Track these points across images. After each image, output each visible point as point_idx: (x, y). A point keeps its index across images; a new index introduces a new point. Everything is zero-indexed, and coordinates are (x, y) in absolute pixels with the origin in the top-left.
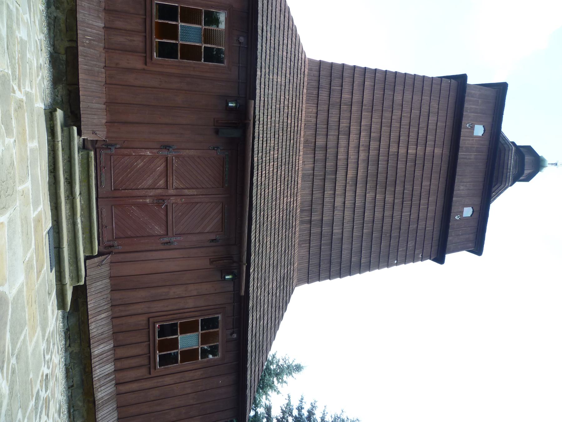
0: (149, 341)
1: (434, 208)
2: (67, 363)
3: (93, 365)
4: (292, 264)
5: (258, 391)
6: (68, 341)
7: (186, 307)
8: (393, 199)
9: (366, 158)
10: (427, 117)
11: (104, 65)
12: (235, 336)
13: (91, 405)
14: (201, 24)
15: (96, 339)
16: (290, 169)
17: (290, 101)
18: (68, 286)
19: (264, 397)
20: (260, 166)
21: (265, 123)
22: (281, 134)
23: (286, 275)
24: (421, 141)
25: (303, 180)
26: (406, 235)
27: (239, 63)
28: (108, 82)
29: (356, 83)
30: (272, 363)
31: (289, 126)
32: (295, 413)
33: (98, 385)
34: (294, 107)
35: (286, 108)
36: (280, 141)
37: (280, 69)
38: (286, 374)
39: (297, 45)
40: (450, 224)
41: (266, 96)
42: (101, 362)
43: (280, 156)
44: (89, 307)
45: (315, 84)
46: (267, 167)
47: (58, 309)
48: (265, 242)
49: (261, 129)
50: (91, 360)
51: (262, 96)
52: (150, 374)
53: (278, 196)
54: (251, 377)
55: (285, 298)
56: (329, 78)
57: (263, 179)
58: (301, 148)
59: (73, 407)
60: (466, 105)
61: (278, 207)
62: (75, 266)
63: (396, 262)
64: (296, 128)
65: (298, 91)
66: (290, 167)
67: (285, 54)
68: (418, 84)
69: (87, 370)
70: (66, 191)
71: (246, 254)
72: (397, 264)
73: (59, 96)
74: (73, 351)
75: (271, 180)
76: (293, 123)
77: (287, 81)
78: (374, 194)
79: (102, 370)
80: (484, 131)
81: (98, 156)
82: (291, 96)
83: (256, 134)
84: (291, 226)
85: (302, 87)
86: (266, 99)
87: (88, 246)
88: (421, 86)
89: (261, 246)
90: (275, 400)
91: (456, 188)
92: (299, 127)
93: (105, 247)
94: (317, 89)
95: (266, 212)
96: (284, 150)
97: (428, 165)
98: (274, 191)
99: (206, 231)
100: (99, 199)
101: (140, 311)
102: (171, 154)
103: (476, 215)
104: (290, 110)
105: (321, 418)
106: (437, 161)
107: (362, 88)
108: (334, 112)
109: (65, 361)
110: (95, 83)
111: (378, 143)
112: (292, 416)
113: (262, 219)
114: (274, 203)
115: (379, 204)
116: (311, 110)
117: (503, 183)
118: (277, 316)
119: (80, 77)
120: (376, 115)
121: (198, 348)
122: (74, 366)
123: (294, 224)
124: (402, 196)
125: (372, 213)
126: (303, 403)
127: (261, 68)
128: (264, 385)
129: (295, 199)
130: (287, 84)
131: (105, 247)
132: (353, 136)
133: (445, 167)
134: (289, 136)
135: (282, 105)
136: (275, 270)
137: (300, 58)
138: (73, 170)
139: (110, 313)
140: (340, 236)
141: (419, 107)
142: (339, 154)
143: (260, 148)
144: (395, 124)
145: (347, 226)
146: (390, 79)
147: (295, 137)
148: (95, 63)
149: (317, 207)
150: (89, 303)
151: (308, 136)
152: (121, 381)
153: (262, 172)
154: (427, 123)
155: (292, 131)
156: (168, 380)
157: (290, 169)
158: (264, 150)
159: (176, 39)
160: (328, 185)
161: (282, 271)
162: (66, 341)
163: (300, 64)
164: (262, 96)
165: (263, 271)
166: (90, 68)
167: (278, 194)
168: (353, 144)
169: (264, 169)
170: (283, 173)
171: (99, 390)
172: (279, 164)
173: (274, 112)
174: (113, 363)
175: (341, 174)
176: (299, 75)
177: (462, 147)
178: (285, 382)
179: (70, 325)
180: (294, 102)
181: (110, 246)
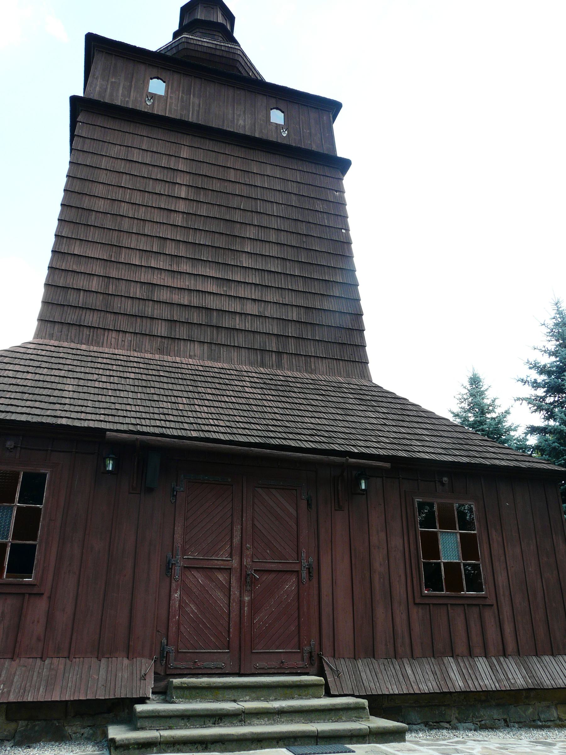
0: (447, 605)
1: (269, 167)
2: (473, 727)
3: (479, 689)
4: (339, 385)
5: (506, 441)
6: (442, 724)
7: (401, 548)
8: (252, 227)
9: (190, 263)
10: (134, 164)
11: (39, 661)
12: (445, 479)
13: (532, 694)
15: (442, 683)
16: (203, 379)
17: (101, 372)
18: (372, 725)
19: (512, 433)
20: (203, 428)
21: (138, 415)
22: (152, 391)
23: (356, 396)
24: (168, 176)
25: (218, 360)
26: (306, 211)
27: (47, 450)
28: (66, 654)
29: (75, 268)
30: (466, 419)
31: (139, 376)
32: (541, 392)
33: (505, 683)
34: (110, 367)
35: (112, 379)
36: (162, 392)
37: (54, 386)
38: (483, 399)
39: (14, 355)
40: (294, 145)
41: (97, 411)
42: (473, 677)
43: (185, 394)
44: (396, 692)
45: (73, 330)
46: (204, 415)
47: (404, 741)
48: (312, 426)
49: (148, 422)
50: (472, 691)
51: (98, 417)
52: (492, 605)
53: (244, 401)
54: (503, 459)
55: (390, 400)
56: (66, 308)
57: (221, 423)
58: (170, 359)
59: (534, 721)
60: (118, 102)
61: (259, 403)
62: (341, 713)
63: (343, 231)
64: (141, 366)
65: (85, 359)
66: (199, 378)
67: (29, 376)
68: (82, 173)
69: (483, 698)
70: (232, 725)
71: (332, 457)
72: (347, 230)
73: (83, 731)
74: (456, 718)
75: (221, 411)
76: (134, 370)
77: (70, 375)
78: (244, 255)
79: (485, 675)
80: (158, 78)
81: (179, 672)
82: (93, 371)
83: (157, 431)
84: (286, 383)
85: (79, 352)
86: (102, 411)
87: (311, 691)
88: (85, 168)
89: (319, 433)
90: (522, 419)
91: (241, 131)
92: (139, 360)
93: (312, 664)
94: (82, 328)
95: (268, 422)
96: (175, 387)
97: (205, 170)
98: (237, 406)
99: (294, 513)
100: (242, 672)
101: (404, 616)
102: (180, 562)
103: (282, 105)
104: (115, 374)
105: (550, 355)
106: (200, 155)
107: (83, 260)
108: (117, 305)
109: (471, 730)
110: (67, 675)
111: (168, 242)
112: (545, 397)
113: (280, 429)
114: (255, 408)
115: (258, 248)
116: (113, 340)
117: (236, 57)
118: (415, 413)
119: (58, 699)
120: (126, 241)
121: (460, 533)
122: (477, 718)
123: (282, 378)
124: (249, 213)
125: (272, 259)
126: (529, 379)
127: (55, 417)
128: (495, 433)
129: (245, 374)
130: (75, 375)
131: (312, 664)
132: (156, 279)
133: (209, 145)
134: (154, 378)
135: (108, 386)
136: (351, 412)
137: (35, 352)
138: (202, 713)
139: (405, 661)
140: (303, 310)
141: (118, 174)
142: (182, 302)
143: (177, 425)
144: (141, 213)
145: (288, 298)
146: (72, 215)
147: (155, 367)
148: (35, 674)
149: (258, 342)
150: (391, 692)
151: (152, 348)
152: (501, 647)
153: (211, 425)
154: (142, 165)
155: (146, 372)
156: (501, 579)
157: (203, 379)
158: (179, 419)
159: (4, 545)
160: (227, 322)
161: (351, 401)
162: (443, 728)
163: (44, 353)
164: (98, 417)
165: (353, 431)
166: (43, 683)
167: (240, 401)
168: (168, 281)
169: (207, 422)
170: (209, 391)
171: (513, 681)
172: (196, 396)
173: (120, 400)
174: (476, 659)
175: (212, 302)
176: (61, 355)
177: (181, 115)
178: (493, 401)
179: (419, 721)
180: (102, 366)
181: (311, 657)
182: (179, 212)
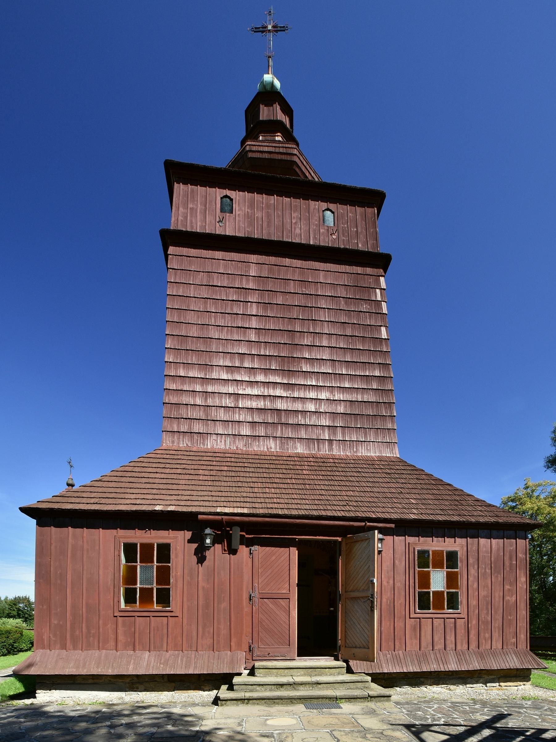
14: (136, 567)
31: (231, 469)
34: (211, 463)
64: (233, 460)
66: (272, 466)
91: (297, 240)
142: (259, 407)
155: (235, 464)
169: (272, 500)
170: (278, 476)
175: (280, 405)
176: (179, 457)
177: (269, 234)
182: (252, 328)
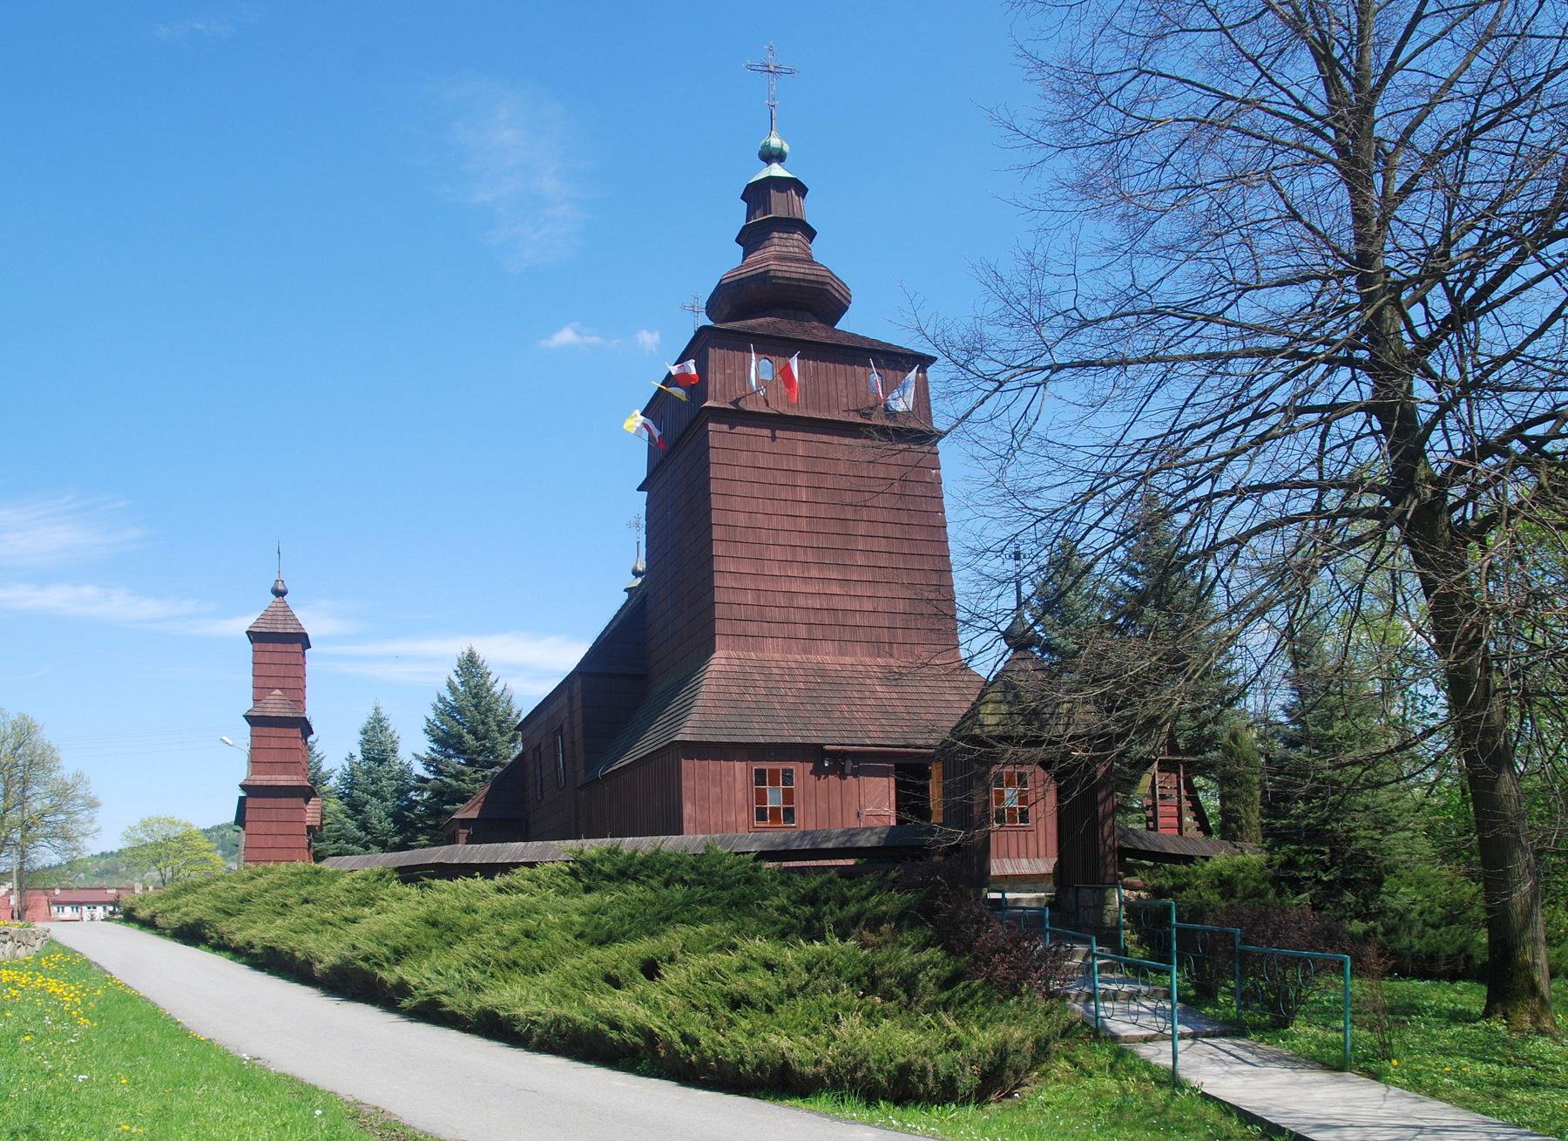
175: (837, 603)
